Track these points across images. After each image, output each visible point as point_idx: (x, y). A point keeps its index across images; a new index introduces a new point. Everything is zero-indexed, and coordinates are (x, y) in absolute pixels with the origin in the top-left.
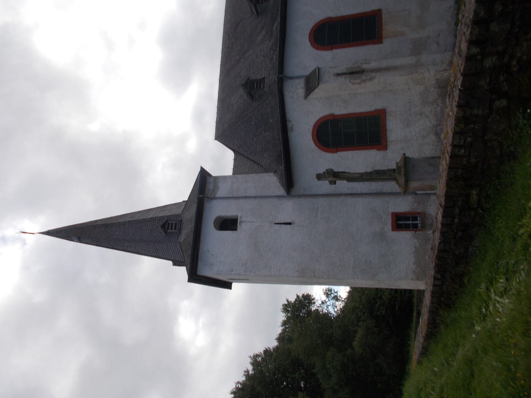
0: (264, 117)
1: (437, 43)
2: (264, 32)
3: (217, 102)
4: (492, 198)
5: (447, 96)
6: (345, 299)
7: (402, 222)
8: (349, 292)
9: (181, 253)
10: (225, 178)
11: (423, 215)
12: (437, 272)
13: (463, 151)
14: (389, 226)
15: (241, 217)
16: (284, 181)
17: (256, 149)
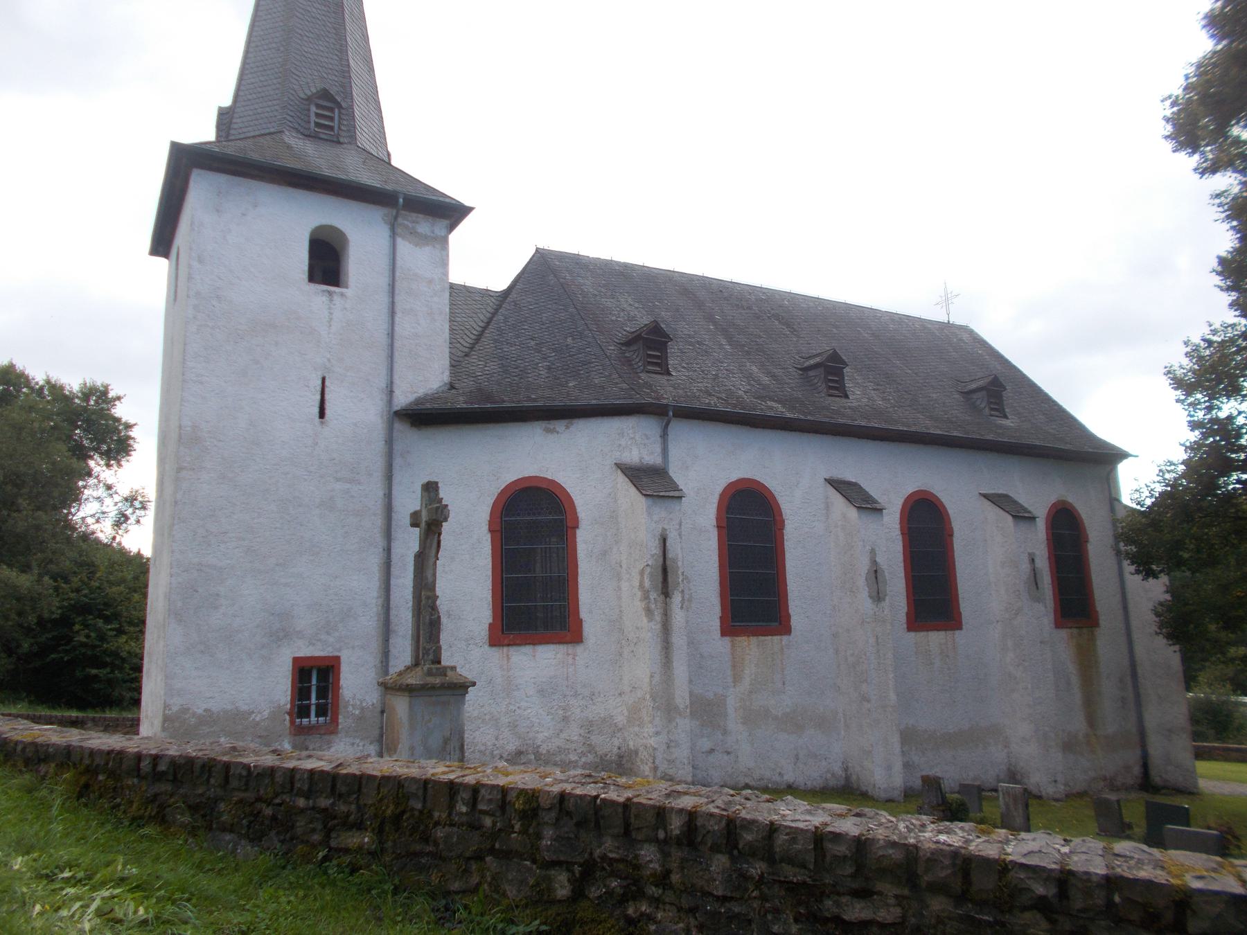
0: (580, 368)
1: (712, 751)
2: (766, 380)
3: (622, 261)
4: (350, 878)
5: (588, 772)
6: (119, 544)
7: (314, 681)
8: (139, 555)
9: (252, 134)
10: (444, 263)
11: (332, 728)
12: (173, 762)
13: (464, 809)
14: (306, 651)
15: (342, 295)
16: (428, 406)
17: (508, 343)
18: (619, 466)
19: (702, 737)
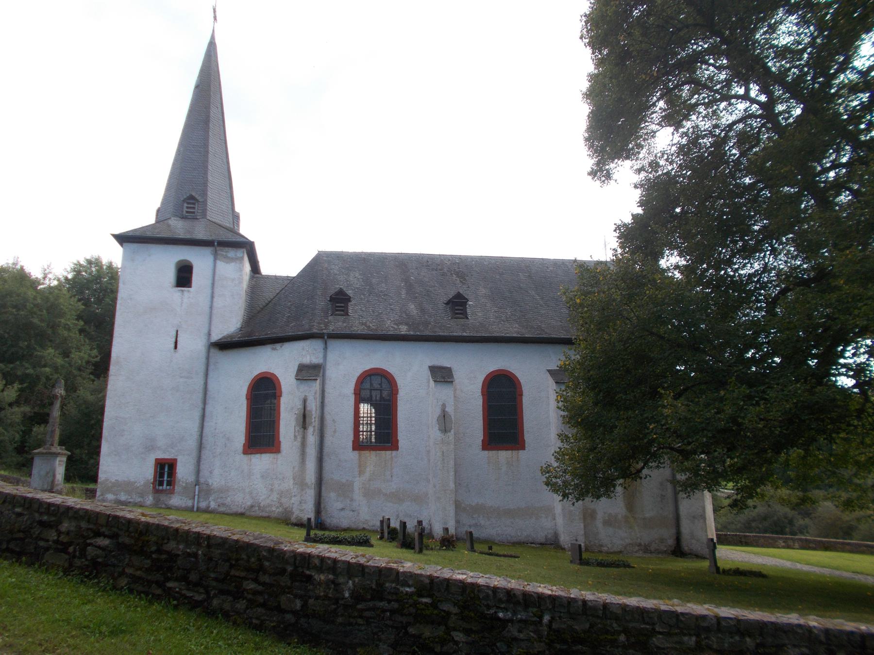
1: (343, 509)
3: (552, 258)
11: (172, 492)
15: (189, 291)
18: (549, 371)
19: (338, 501)
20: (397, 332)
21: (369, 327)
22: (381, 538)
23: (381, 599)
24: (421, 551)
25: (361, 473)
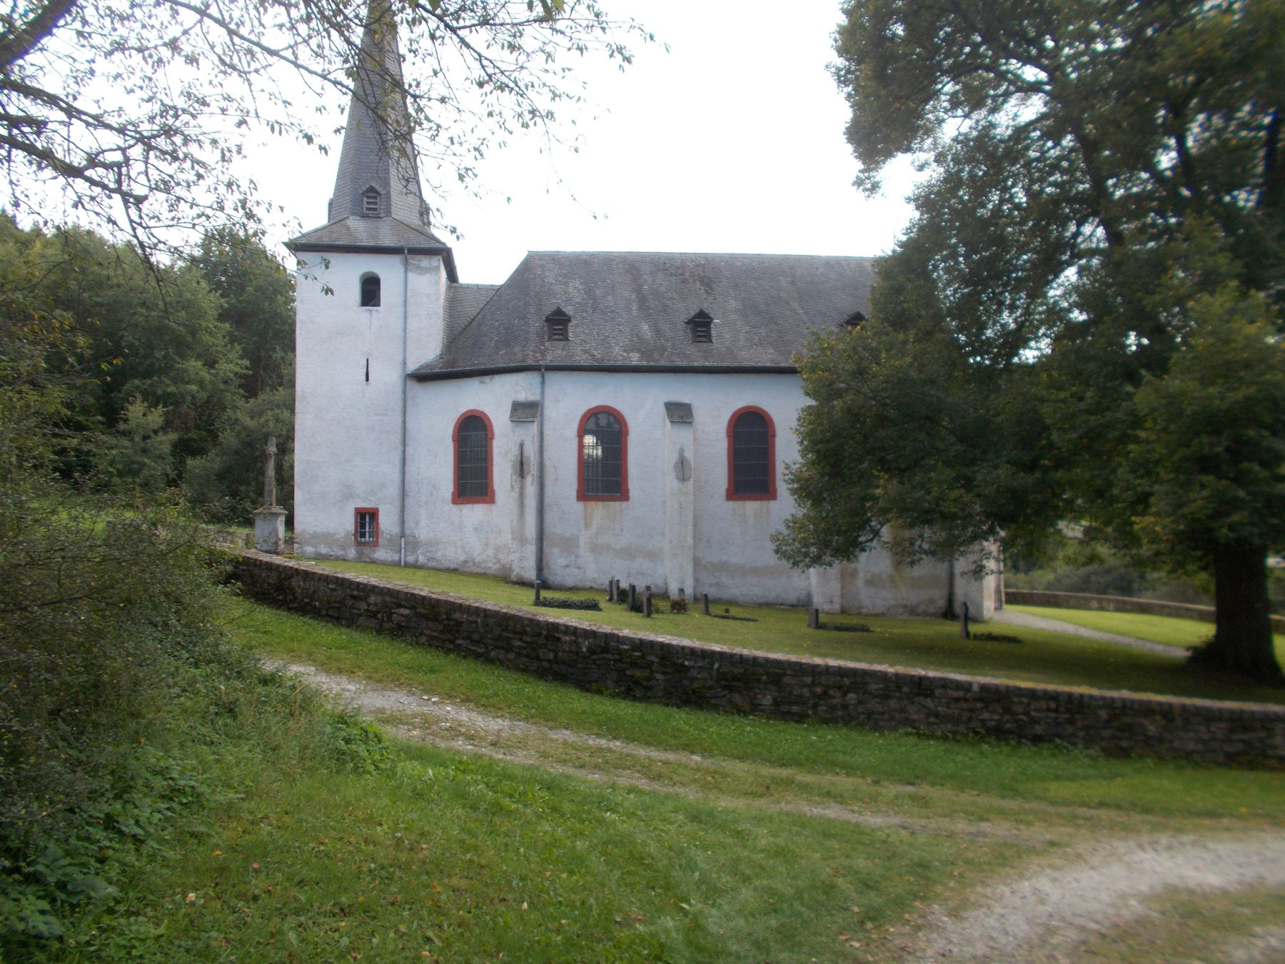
20: (627, 363)
21: (593, 356)
22: (611, 600)
23: (607, 653)
24: (649, 615)
25: (587, 526)
